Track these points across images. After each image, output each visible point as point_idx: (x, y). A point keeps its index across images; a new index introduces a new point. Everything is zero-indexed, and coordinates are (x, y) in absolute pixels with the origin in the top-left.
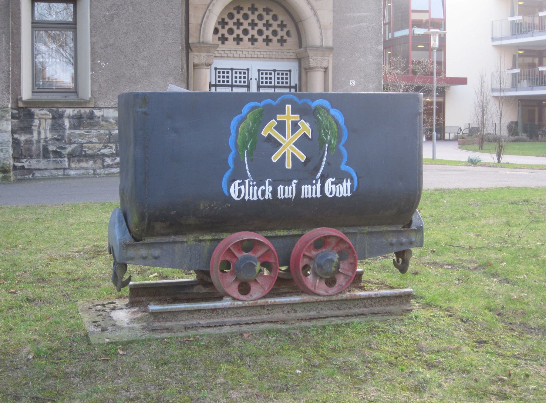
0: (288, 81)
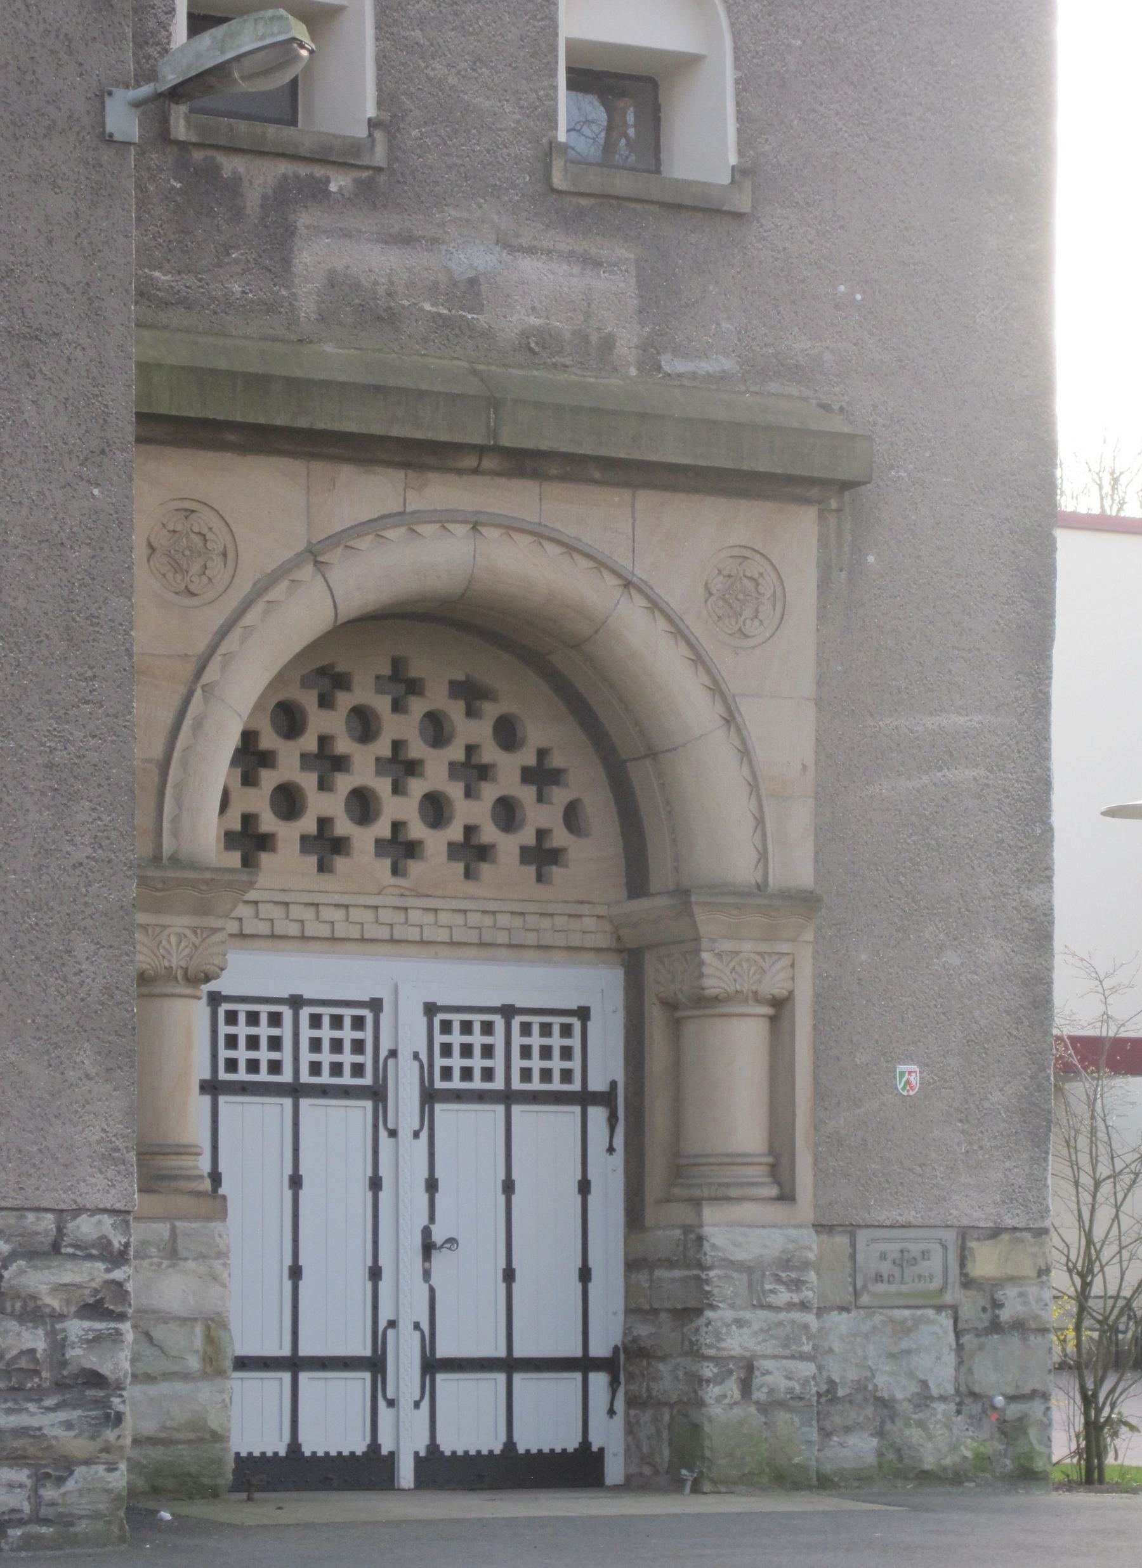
0: (575, 1065)
